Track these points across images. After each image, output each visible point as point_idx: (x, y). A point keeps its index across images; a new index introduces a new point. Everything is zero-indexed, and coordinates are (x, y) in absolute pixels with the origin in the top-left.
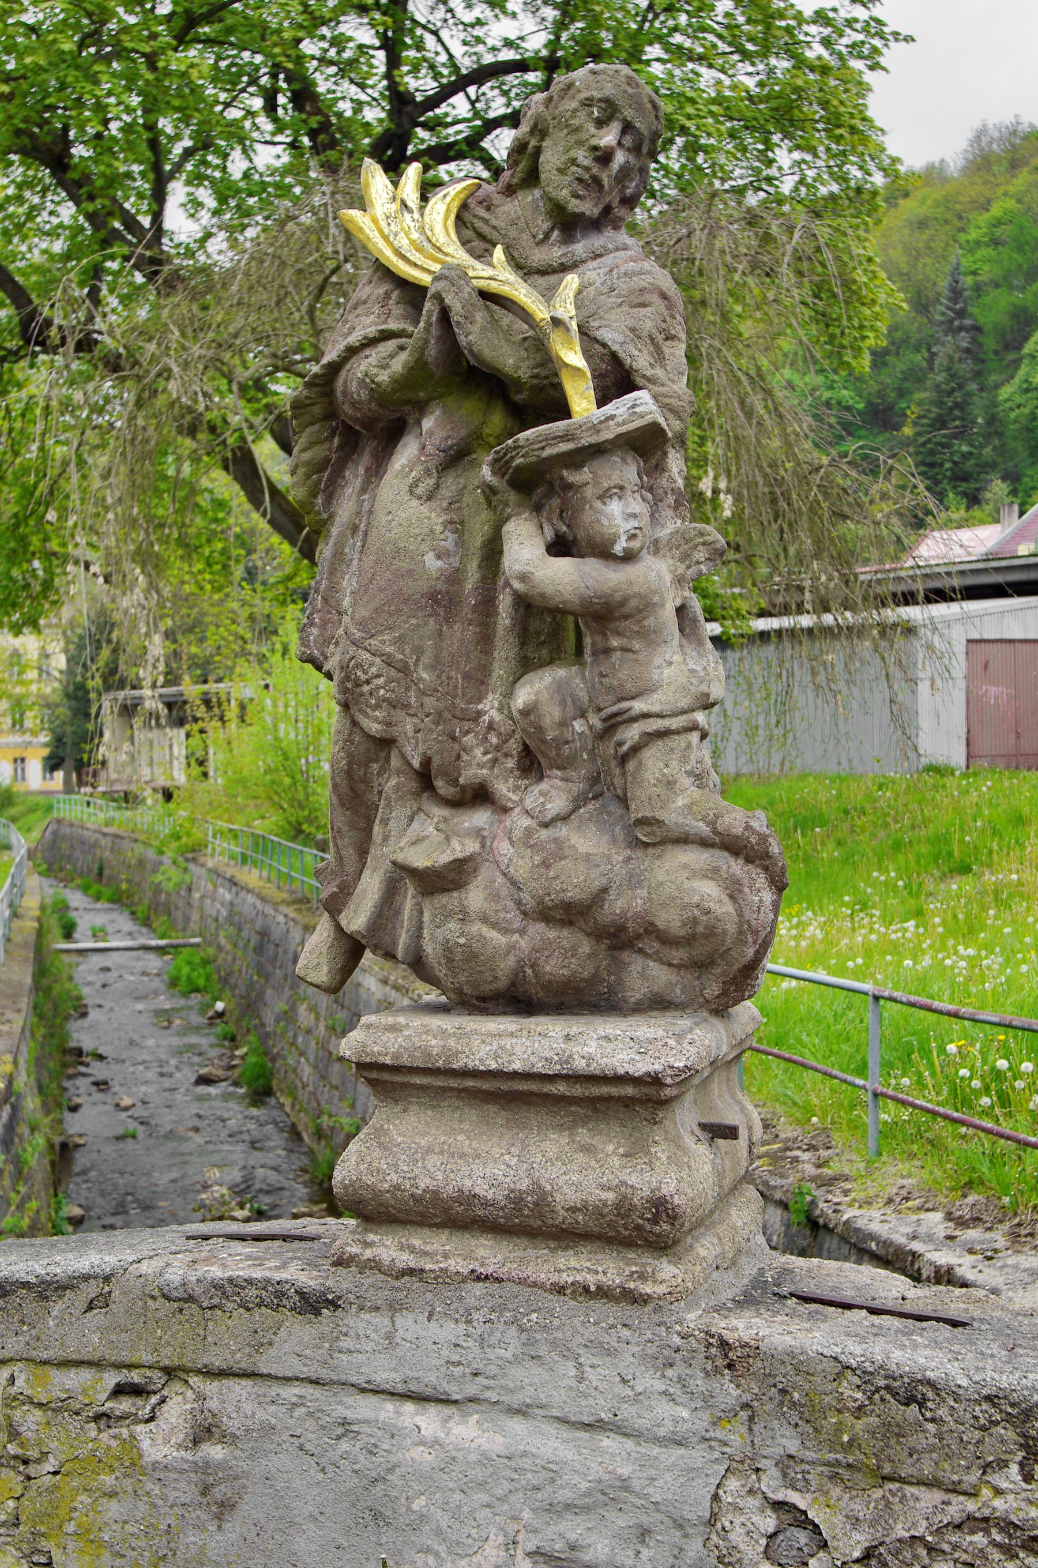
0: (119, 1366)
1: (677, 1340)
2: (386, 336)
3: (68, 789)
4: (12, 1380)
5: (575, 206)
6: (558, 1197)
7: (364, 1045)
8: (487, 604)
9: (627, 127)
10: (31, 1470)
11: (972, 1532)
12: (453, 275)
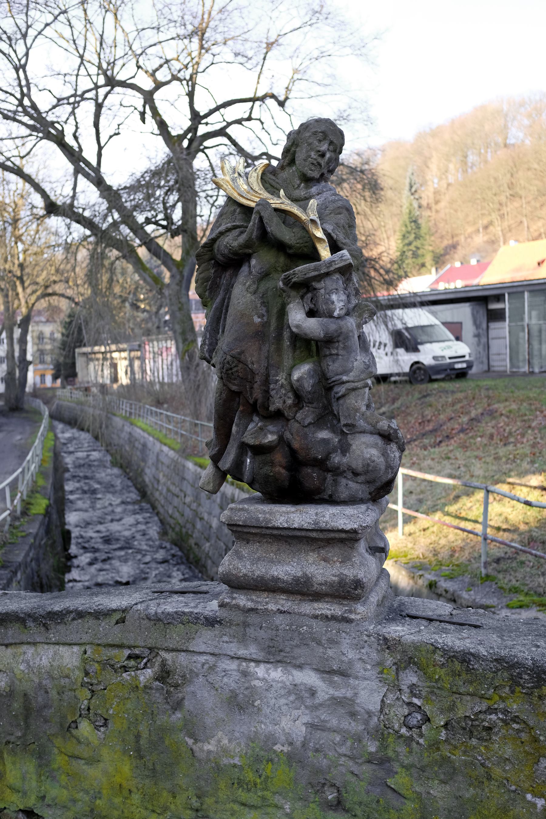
0: (129, 647)
1: (366, 638)
2: (235, 227)
3: (63, 387)
4: (85, 652)
5: (310, 174)
6: (314, 579)
7: (231, 517)
8: (279, 338)
9: (331, 143)
10: (95, 688)
11: (490, 714)
12: (263, 203)
